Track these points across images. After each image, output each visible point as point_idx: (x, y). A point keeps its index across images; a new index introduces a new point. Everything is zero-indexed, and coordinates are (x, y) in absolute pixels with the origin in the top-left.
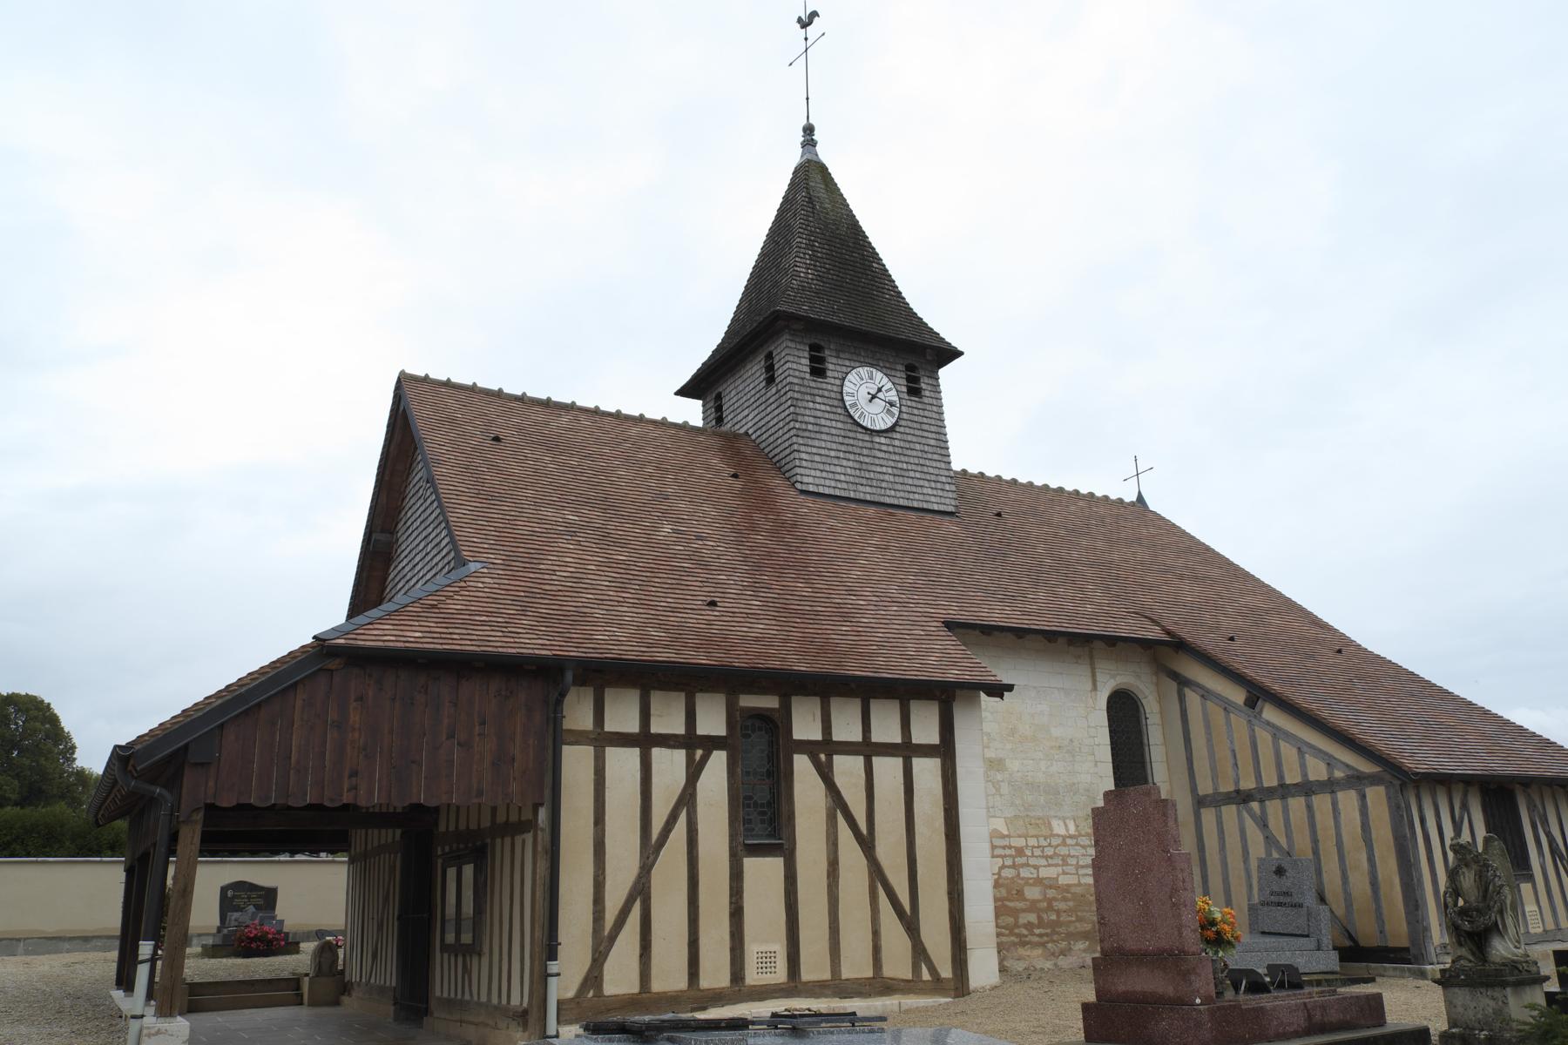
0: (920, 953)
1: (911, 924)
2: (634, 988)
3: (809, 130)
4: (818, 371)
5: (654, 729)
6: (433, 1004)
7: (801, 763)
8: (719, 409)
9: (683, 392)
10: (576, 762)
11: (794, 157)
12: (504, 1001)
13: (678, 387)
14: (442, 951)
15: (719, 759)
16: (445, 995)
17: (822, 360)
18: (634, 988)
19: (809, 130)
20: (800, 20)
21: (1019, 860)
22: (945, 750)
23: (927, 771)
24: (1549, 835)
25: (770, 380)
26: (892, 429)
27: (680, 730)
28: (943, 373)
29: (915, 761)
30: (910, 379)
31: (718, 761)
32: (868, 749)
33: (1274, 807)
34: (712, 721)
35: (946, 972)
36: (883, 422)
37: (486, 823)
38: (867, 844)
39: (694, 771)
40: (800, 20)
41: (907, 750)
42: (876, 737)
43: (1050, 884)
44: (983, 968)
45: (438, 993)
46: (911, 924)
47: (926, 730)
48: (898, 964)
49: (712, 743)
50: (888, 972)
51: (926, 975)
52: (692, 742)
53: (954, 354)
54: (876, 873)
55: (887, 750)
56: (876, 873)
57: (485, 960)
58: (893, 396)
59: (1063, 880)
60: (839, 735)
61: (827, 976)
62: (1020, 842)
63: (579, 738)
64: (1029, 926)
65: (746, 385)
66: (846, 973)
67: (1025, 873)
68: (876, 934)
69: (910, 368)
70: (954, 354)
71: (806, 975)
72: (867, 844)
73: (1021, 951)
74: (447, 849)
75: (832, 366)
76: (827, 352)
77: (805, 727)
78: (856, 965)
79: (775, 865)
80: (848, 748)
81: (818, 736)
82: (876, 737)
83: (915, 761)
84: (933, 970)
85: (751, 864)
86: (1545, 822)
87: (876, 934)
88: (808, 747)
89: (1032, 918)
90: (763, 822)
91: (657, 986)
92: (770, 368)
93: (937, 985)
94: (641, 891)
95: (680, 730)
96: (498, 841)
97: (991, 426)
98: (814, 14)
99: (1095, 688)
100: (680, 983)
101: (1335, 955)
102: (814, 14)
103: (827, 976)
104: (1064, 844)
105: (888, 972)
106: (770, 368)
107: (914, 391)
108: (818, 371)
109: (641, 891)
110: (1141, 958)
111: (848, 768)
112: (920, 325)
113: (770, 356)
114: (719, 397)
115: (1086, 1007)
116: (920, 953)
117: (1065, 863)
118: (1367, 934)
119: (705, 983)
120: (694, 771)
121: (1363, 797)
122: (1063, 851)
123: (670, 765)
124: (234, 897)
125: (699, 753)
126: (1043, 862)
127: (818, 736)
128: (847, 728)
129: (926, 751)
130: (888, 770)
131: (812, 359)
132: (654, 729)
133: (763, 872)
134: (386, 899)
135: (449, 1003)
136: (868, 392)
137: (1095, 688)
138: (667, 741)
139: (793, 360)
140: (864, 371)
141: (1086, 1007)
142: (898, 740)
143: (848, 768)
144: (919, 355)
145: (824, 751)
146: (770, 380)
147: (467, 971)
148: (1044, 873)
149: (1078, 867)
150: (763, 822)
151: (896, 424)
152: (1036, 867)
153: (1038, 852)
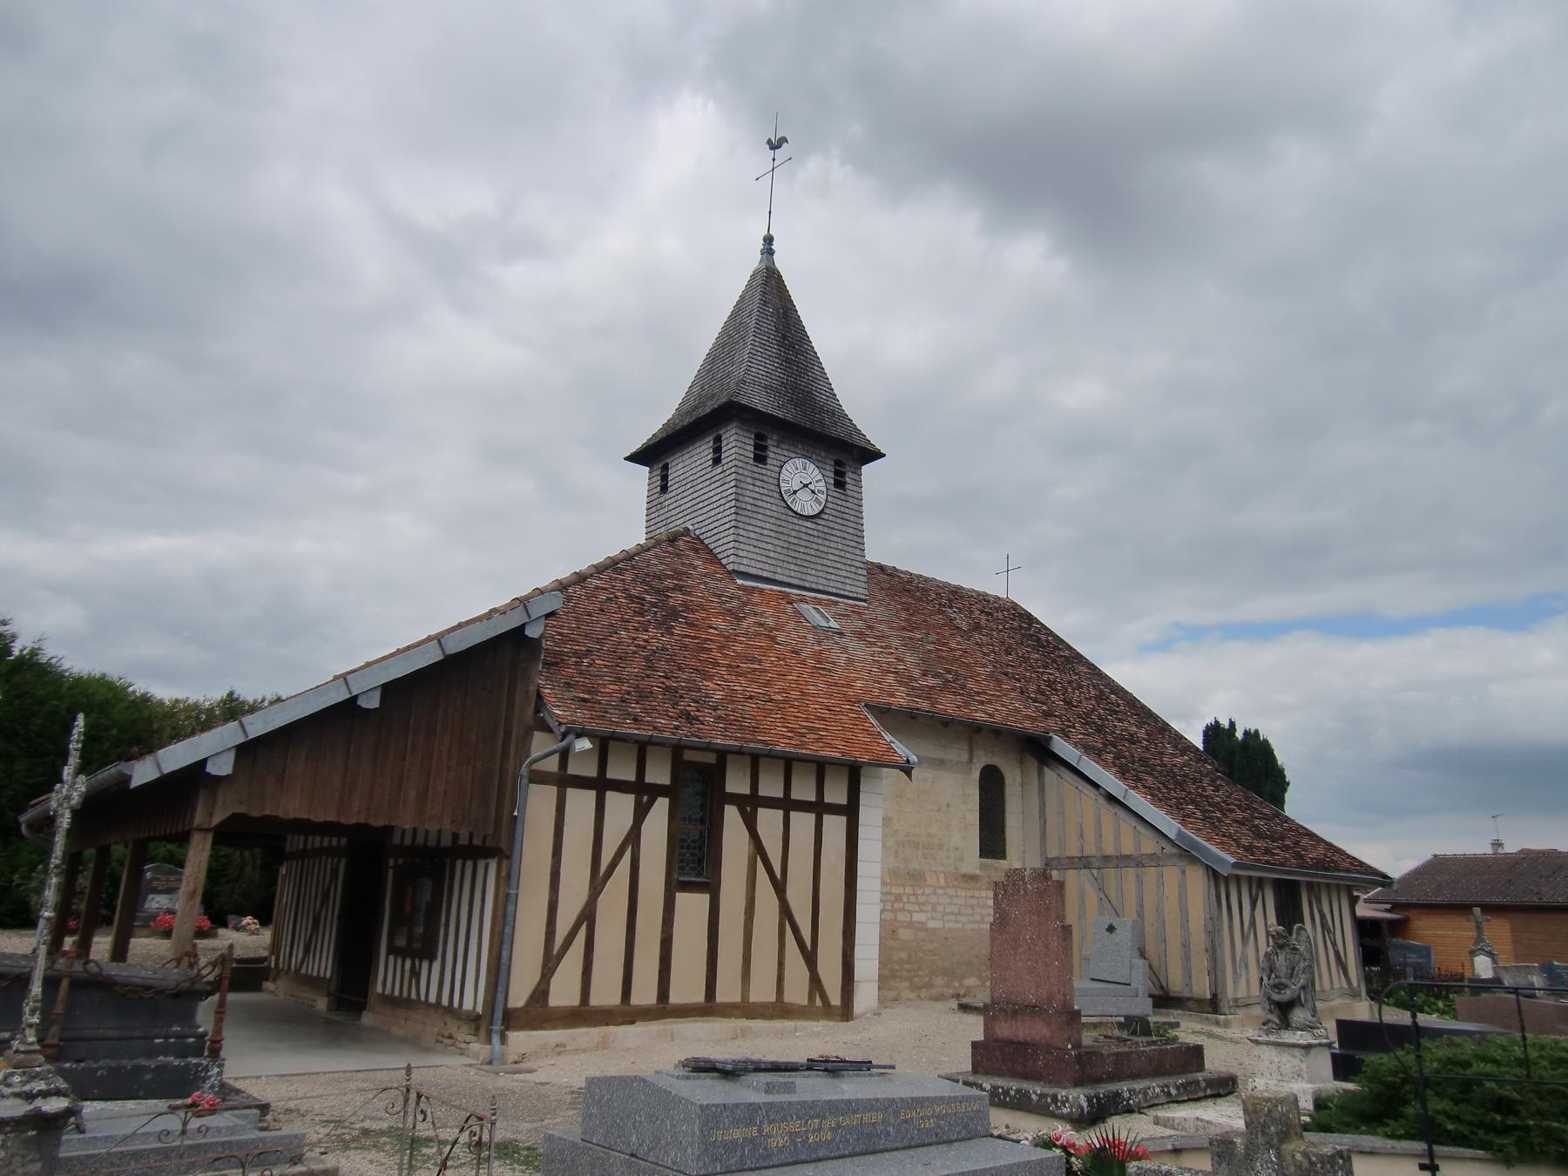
0: (815, 982)
1: (810, 958)
2: (575, 1001)
3: (769, 240)
4: (760, 458)
5: (610, 775)
6: (372, 1000)
7: (731, 814)
8: (665, 478)
9: (635, 458)
10: (539, 803)
11: (754, 260)
12: (456, 1003)
13: (636, 445)
14: (389, 952)
15: (662, 805)
16: (388, 991)
17: (765, 448)
18: (576, 1002)
19: (769, 240)
20: (769, 142)
21: (896, 905)
22: (851, 811)
23: (835, 826)
24: (1323, 916)
25: (717, 461)
26: (817, 516)
27: (632, 777)
28: (867, 469)
29: (826, 817)
30: (837, 473)
31: (662, 805)
32: (787, 805)
33: (1111, 874)
34: (659, 774)
35: (836, 1000)
36: (811, 509)
37: (446, 841)
38: (780, 887)
39: (641, 813)
40: (769, 142)
41: (819, 808)
42: (795, 796)
43: (921, 927)
44: (866, 994)
45: (379, 989)
46: (810, 958)
47: (836, 794)
48: (797, 992)
49: (657, 791)
50: (788, 997)
51: (818, 1002)
52: (644, 793)
53: (878, 455)
54: (786, 912)
55: (803, 806)
56: (786, 912)
57: (437, 965)
58: (821, 486)
59: (932, 924)
60: (764, 791)
61: (738, 999)
62: (899, 890)
63: (540, 778)
64: (901, 962)
65: (691, 464)
66: (753, 998)
67: (901, 917)
68: (781, 964)
69: (838, 463)
70: (878, 455)
71: (721, 997)
72: (780, 887)
73: (893, 983)
74: (400, 861)
75: (773, 453)
76: (769, 442)
77: (737, 783)
78: (762, 992)
79: (703, 899)
80: (771, 803)
81: (747, 791)
82: (795, 796)
83: (826, 817)
84: (824, 997)
85: (682, 898)
86: (1319, 901)
87: (781, 964)
88: (737, 800)
89: (903, 955)
90: (694, 863)
91: (595, 1001)
92: (717, 450)
93: (828, 1012)
94: (588, 916)
95: (632, 777)
96: (459, 863)
97: (900, 526)
98: (783, 140)
99: (971, 760)
100: (615, 999)
101: (1150, 1001)
102: (783, 140)
103: (738, 999)
104: (935, 893)
105: (788, 997)
106: (717, 450)
107: (840, 484)
108: (760, 458)
109: (588, 916)
110: (1018, 1010)
111: (769, 821)
112: (839, 415)
113: (718, 439)
114: (666, 468)
115: (975, 1045)
116: (815, 982)
117: (934, 910)
118: (1176, 985)
119: (635, 1000)
120: (641, 813)
121: (1183, 872)
122: (933, 899)
123: (620, 807)
124: (154, 879)
125: (645, 798)
126: (916, 908)
127: (747, 791)
128: (771, 787)
129: (835, 809)
130: (803, 823)
131: (757, 447)
132: (610, 775)
133: (692, 905)
134: (326, 896)
135: (390, 1001)
136: (802, 477)
137: (971, 760)
138: (621, 786)
139: (736, 443)
140: (799, 462)
141: (975, 1045)
142: (813, 799)
143: (769, 821)
144: (847, 453)
145: (750, 805)
146: (717, 461)
147: (415, 974)
148: (917, 917)
149: (945, 914)
150: (694, 863)
151: (822, 512)
152: (910, 912)
153: (912, 899)
